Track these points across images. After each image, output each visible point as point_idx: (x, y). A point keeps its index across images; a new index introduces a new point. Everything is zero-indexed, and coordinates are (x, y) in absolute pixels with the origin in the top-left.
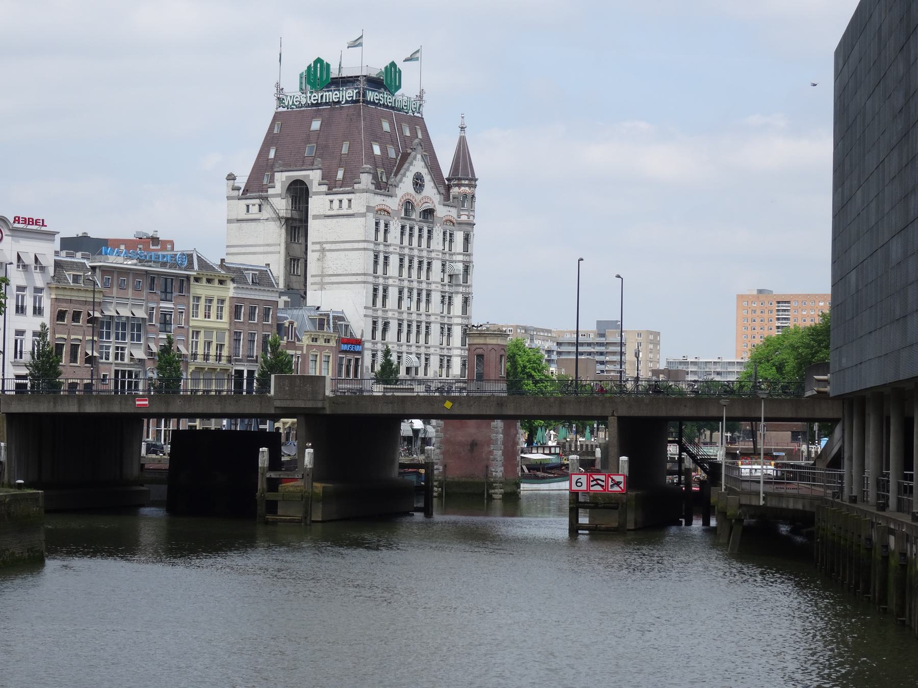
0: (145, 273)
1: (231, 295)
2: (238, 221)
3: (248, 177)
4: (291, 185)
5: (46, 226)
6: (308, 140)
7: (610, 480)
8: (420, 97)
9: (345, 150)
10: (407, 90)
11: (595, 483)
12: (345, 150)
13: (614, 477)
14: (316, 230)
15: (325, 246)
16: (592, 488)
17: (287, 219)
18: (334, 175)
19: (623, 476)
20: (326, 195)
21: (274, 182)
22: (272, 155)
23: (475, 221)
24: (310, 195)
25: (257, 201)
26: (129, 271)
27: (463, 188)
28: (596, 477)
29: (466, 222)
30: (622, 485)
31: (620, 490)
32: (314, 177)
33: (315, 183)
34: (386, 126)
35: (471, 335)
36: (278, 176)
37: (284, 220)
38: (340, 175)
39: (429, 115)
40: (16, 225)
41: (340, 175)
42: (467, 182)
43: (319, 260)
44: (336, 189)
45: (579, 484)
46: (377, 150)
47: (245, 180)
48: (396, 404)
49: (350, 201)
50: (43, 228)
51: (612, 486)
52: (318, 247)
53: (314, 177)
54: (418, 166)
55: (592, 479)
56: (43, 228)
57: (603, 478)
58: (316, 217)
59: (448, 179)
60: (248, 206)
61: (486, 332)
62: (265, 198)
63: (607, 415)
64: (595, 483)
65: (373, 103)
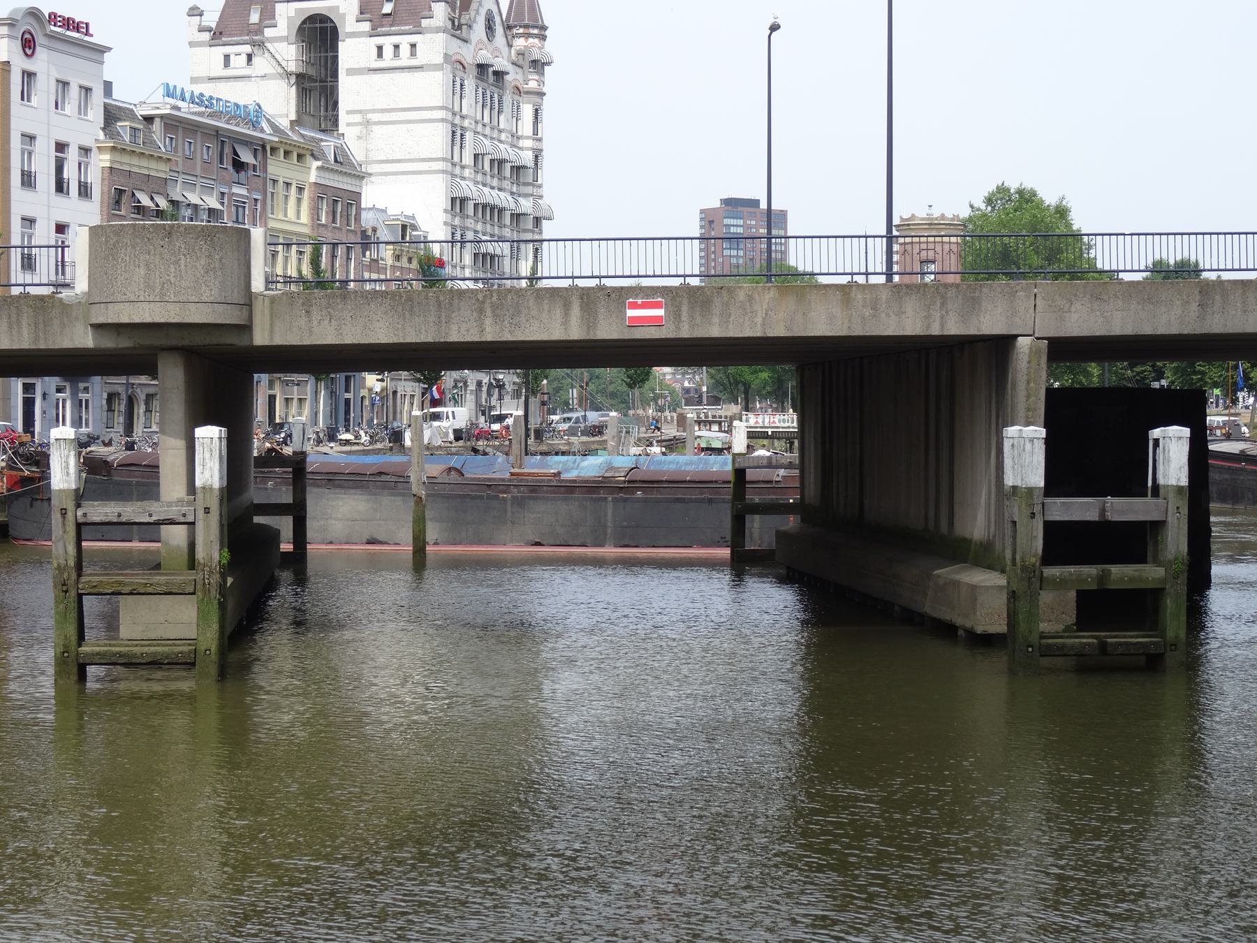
0: (214, 133)
1: (313, 179)
2: (211, 79)
3: (219, 14)
4: (304, 22)
5: (91, 35)
14: (350, 91)
15: (369, 116)
17: (300, 76)
18: (377, 7)
20: (370, 36)
21: (274, 19)
23: (544, 90)
24: (341, 37)
25: (248, 49)
26: (196, 129)
27: (531, 40)
29: (536, 90)
35: (911, 227)
37: (294, 77)
42: (521, 31)
43: (359, 138)
44: (383, 29)
47: (216, 17)
49: (413, 46)
50: (87, 38)
52: (358, 118)
56: (87, 38)
58: (350, 72)
60: (227, 57)
61: (942, 222)
62: (260, 45)
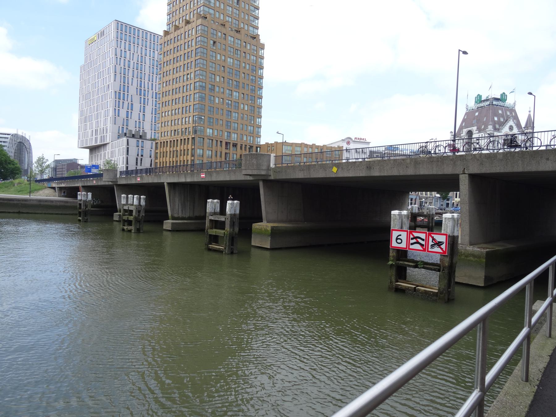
6: (474, 119)
7: (431, 239)
8: (515, 104)
9: (485, 120)
10: (510, 101)
11: (414, 241)
12: (485, 120)
13: (435, 236)
16: (411, 247)
19: (445, 236)
22: (464, 125)
27: (529, 130)
28: (416, 235)
30: (443, 246)
31: (442, 252)
32: (474, 129)
33: (475, 130)
34: (500, 112)
36: (464, 130)
38: (483, 127)
39: (517, 109)
40: (356, 140)
41: (483, 127)
45: (399, 241)
46: (496, 119)
48: (305, 171)
51: (432, 246)
53: (474, 129)
54: (511, 123)
55: (411, 236)
57: (423, 236)
59: (524, 128)
63: (457, 172)
64: (414, 241)
65: (496, 105)
